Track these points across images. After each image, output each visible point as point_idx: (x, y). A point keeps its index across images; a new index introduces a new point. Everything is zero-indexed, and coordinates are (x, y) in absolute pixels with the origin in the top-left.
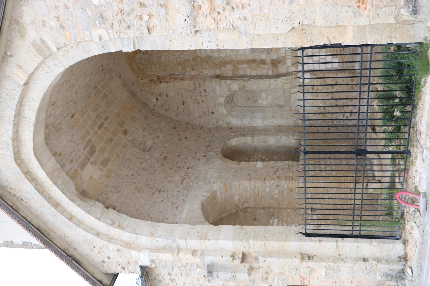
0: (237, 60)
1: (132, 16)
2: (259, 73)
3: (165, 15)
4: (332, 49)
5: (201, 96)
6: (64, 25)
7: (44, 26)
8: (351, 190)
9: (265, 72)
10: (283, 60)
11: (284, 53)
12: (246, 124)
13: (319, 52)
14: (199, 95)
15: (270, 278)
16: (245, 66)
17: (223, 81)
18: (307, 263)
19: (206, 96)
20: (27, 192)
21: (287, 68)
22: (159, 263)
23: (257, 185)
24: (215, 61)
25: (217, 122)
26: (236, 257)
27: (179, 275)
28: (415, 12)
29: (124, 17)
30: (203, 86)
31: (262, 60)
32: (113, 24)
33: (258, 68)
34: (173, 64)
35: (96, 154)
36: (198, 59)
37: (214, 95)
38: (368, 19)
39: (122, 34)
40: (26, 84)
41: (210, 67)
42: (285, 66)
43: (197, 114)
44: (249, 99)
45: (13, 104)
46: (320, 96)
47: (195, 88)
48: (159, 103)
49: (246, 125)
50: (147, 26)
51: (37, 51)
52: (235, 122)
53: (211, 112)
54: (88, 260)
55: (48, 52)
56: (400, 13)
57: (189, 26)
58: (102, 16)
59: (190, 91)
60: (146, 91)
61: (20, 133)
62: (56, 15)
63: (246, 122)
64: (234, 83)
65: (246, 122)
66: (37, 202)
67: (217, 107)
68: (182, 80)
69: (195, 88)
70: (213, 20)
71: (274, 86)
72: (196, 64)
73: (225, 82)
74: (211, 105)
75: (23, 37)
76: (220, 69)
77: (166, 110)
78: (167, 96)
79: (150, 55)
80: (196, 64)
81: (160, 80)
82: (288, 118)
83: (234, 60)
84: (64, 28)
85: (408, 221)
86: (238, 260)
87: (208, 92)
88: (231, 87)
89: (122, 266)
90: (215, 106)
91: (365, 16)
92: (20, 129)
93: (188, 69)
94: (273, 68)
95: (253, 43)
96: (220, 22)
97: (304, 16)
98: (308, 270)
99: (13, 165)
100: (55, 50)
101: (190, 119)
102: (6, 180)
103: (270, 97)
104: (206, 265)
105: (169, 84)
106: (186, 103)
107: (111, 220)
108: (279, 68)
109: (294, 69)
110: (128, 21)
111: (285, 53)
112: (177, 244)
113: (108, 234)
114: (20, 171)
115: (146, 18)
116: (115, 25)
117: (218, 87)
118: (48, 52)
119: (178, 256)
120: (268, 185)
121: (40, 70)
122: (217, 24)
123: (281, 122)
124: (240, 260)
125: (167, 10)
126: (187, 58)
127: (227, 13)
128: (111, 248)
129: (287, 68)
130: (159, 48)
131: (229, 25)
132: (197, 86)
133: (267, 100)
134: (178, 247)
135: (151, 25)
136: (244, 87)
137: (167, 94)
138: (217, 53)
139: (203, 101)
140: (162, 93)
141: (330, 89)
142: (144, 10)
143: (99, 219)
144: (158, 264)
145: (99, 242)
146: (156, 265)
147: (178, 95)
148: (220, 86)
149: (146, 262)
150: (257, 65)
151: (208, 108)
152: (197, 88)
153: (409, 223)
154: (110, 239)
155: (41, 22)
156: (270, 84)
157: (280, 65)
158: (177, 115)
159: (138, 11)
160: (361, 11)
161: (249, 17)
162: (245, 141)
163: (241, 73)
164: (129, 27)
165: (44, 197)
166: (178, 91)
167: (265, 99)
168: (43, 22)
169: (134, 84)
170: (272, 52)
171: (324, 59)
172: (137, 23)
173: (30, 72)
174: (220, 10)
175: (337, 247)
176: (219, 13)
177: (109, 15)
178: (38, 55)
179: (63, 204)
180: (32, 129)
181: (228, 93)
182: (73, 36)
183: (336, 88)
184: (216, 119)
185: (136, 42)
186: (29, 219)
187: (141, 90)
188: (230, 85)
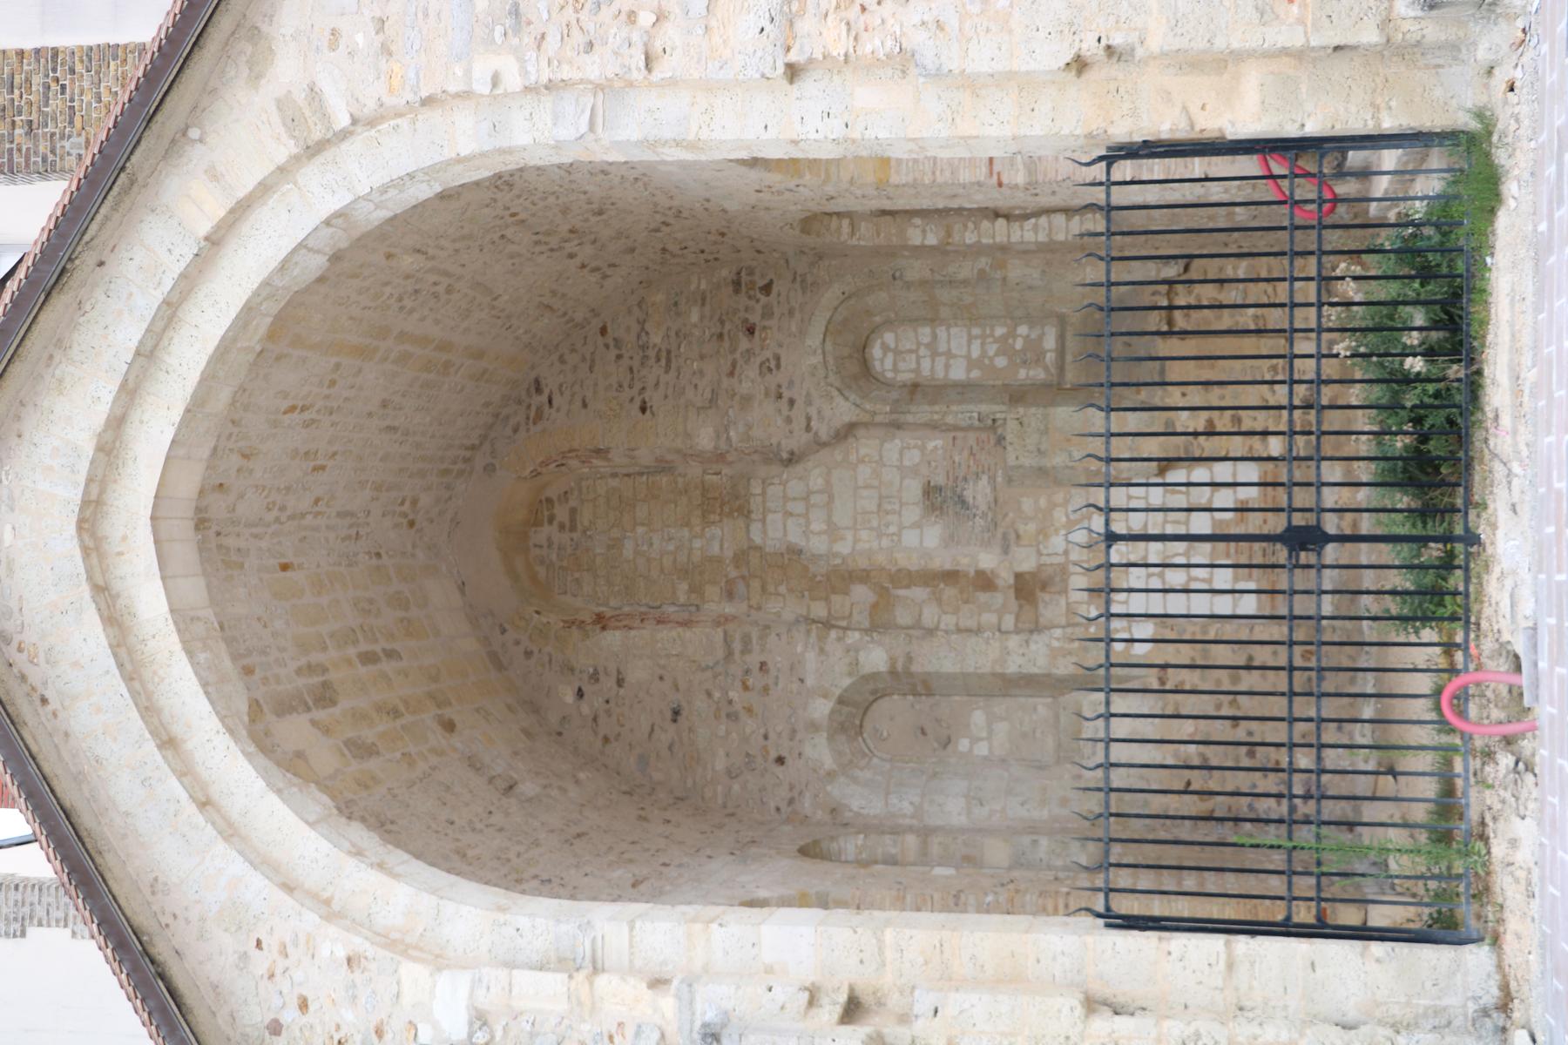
0: (894, 570)
3: (704, 12)
4: (1233, 544)
5: (746, 688)
6: (393, 48)
7: (333, 46)
8: (1275, 653)
10: (1058, 579)
11: (1061, 551)
12: (904, 816)
13: (1186, 554)
14: (738, 684)
16: (919, 593)
19: (766, 690)
20: (76, 664)
22: (505, 1029)
24: (812, 568)
25: (791, 801)
26: (825, 1000)
30: (756, 647)
31: (980, 574)
32: (543, 36)
33: (966, 602)
34: (662, 570)
35: (336, 711)
36: (754, 559)
37: (795, 686)
38: (1301, 29)
39: (565, 67)
41: (791, 590)
42: (1063, 602)
43: (720, 764)
44: (924, 733)
45: (147, 302)
46: (1190, 704)
47: (729, 655)
48: (585, 709)
49: (901, 821)
50: (646, 45)
51: (284, 125)
52: (860, 799)
53: (773, 755)
54: (214, 1014)
55: (319, 127)
56: (1394, 15)
57: (770, 48)
59: (707, 668)
60: (546, 659)
62: (378, 14)
63: (904, 805)
64: (873, 641)
65: (906, 804)
66: (99, 710)
67: (799, 736)
68: (687, 624)
69: (729, 655)
70: (844, 27)
71: (1020, 661)
72: (743, 577)
73: (839, 639)
74: (779, 728)
75: (256, 77)
76: (827, 600)
77: (606, 740)
78: (620, 682)
79: (584, 532)
80: (743, 577)
81: (601, 621)
82: (1064, 802)
83: (883, 569)
84: (390, 54)
85: (1495, 819)
86: (828, 1008)
87: (773, 672)
88: (862, 656)
90: (794, 731)
91: (1291, 20)
92: (135, 416)
93: (712, 591)
94: (1021, 607)
95: (958, 120)
96: (864, 36)
97: (1112, 19)
99: (66, 544)
101: (690, 783)
102: (16, 609)
103: (1002, 728)
104: (698, 1024)
105: (633, 633)
106: (684, 713)
107: (353, 845)
108: (1041, 606)
110: (590, 26)
111: (1066, 553)
112: (594, 940)
113: (326, 895)
114: (82, 570)
115: (645, 19)
116: (548, 38)
117: (811, 657)
118: (319, 127)
119: (591, 984)
121: (270, 202)
122: (856, 39)
124: (838, 1010)
126: (716, 549)
128: (324, 951)
131: (889, 43)
132: (737, 646)
133: (989, 738)
134: (594, 962)
135: (658, 45)
137: (619, 672)
138: (824, 537)
139: (749, 710)
140: (601, 670)
141: (1224, 680)
143: (311, 824)
144: (499, 1034)
145: (289, 920)
146: (493, 1037)
147: (661, 678)
148: (822, 650)
150: (961, 592)
151: (766, 737)
152: (737, 655)
153: (1501, 825)
154: (329, 910)
155: (327, 33)
156: (1006, 652)
157: (1046, 597)
158: (643, 760)
162: (893, 851)
164: (591, 44)
165: (134, 694)
166: (662, 662)
167: (984, 734)
169: (507, 626)
170: (1018, 545)
171: (1196, 579)
173: (241, 194)
175: (1230, 966)
176: (863, 9)
178: (284, 137)
179: (189, 746)
180: (176, 415)
181: (847, 682)
182: (412, 75)
183: (1250, 680)
184: (791, 788)
185: (600, 112)
186: (47, 769)
187: (528, 654)
188: (857, 651)
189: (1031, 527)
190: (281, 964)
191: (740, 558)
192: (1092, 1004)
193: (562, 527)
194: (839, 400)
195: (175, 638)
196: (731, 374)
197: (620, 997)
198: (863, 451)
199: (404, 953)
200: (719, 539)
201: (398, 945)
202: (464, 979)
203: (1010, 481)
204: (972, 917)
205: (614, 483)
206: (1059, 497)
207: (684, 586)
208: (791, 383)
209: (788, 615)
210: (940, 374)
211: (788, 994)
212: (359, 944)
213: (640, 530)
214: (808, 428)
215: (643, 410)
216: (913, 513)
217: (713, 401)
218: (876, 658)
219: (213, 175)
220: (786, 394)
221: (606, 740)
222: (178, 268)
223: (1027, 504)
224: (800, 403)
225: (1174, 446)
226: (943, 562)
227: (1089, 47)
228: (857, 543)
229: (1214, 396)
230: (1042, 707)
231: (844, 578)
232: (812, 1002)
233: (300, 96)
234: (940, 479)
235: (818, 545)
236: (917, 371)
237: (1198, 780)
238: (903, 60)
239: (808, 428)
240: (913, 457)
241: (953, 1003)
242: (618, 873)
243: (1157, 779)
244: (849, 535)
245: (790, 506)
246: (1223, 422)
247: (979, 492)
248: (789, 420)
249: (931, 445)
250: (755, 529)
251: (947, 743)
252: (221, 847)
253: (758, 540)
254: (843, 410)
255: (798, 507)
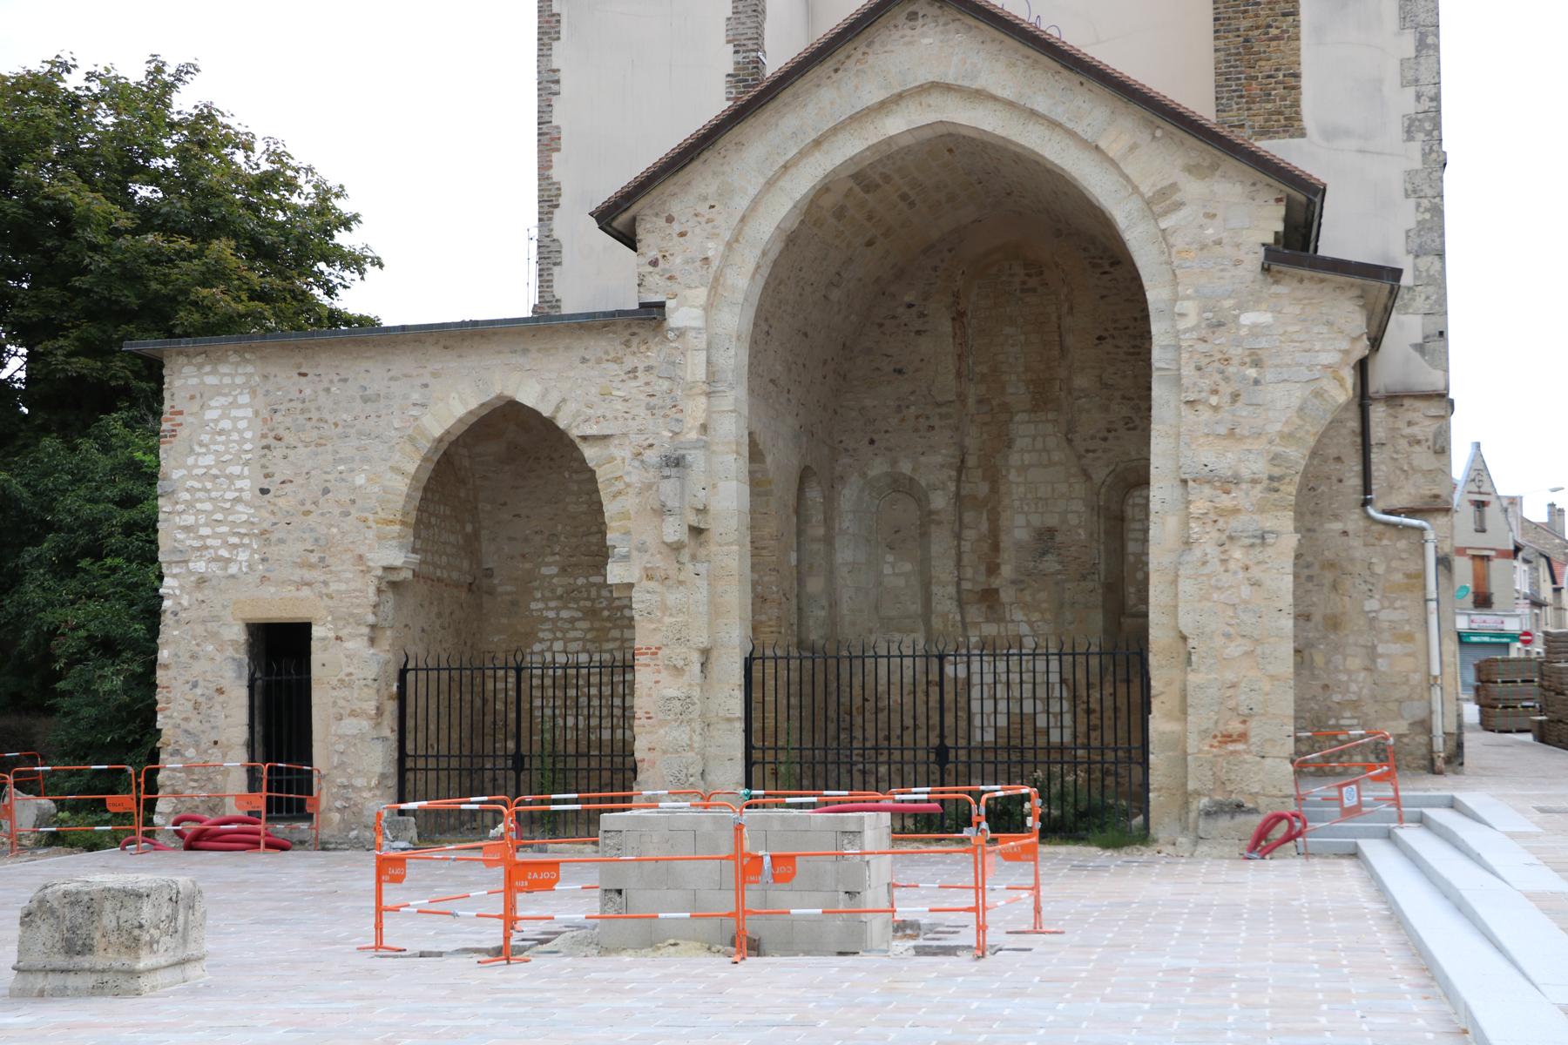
1: (1218, 377)
2: (966, 560)
9: (969, 573)
15: (652, 585)
16: (984, 527)
17: (954, 473)
18: (695, 658)
19: (916, 430)
20: (857, 88)
21: (976, 624)
23: (764, 552)
25: (846, 450)
27: (649, 390)
28: (1208, 814)
29: (1216, 364)
31: (998, 566)
35: (862, 194)
40: (1097, 147)
45: (1059, 114)
46: (908, 700)
47: (939, 405)
52: (848, 496)
53: (875, 437)
58: (1220, 324)
61: (990, 105)
63: (847, 522)
68: (959, 375)
69: (939, 405)
75: (1190, 170)
77: (881, 325)
78: (918, 333)
81: (959, 317)
82: (853, 624)
89: (661, 261)
98: (680, 663)
99: (923, 76)
100: (1163, 225)
109: (973, 640)
115: (1214, 400)
117: (939, 459)
120: (766, 579)
123: (845, 609)
125: (1225, 437)
127: (1215, 535)
129: (976, 624)
130: (1155, 412)
132: (944, 410)
133: (895, 574)
135: (1200, 407)
136: (939, 523)
139: (903, 420)
142: (1227, 399)
145: (725, 224)
148: (942, 466)
149: (678, 317)
159: (1226, 390)
160: (1209, 741)
161: (1206, 570)
163: (968, 517)
168: (1214, 216)
172: (1206, 383)
174: (1221, 524)
175: (729, 720)
177: (1221, 338)
181: (923, 484)
187: (935, 269)
189: (1028, 599)
190: (703, 220)
191: (1005, 407)
192: (706, 653)
193: (1024, 283)
194: (1107, 471)
195: (875, 141)
196: (1123, 397)
197: (696, 409)
198: (1077, 486)
199: (712, 287)
200: (1017, 392)
201: (715, 285)
202: (699, 323)
203: (1057, 583)
204: (109, 999)
205: (1054, 318)
206: (1048, 616)
207: (985, 370)
208: (1117, 438)
209: (968, 441)
210: (1132, 535)
211: (701, 498)
212: (715, 264)
213: (1022, 338)
214: (1088, 451)
215: (1099, 338)
216: (1036, 520)
217: (1106, 386)
218: (939, 501)
219: (1133, 148)
220: (1110, 435)
221: (881, 325)
222: (1079, 130)
223: (1043, 595)
224: (1104, 444)
225: (1082, 692)
226: (1005, 541)
227: (1192, 643)
228: (1016, 485)
229: (1109, 713)
230: (916, 608)
231: (994, 477)
232: (698, 511)
233: (1177, 197)
234: (1059, 538)
235: (1015, 459)
236: (1134, 520)
237: (870, 705)
238: (1188, 543)
239: (1088, 451)
240: (1073, 520)
241: (702, 583)
242: (779, 368)
243: (870, 680)
244: (1020, 479)
245: (1040, 439)
246: (1095, 720)
247: (1051, 564)
248: (1093, 438)
249: (1081, 531)
250: (1025, 417)
251: (891, 547)
252: (762, 181)
253: (1017, 418)
254: (1100, 474)
255: (1039, 445)
